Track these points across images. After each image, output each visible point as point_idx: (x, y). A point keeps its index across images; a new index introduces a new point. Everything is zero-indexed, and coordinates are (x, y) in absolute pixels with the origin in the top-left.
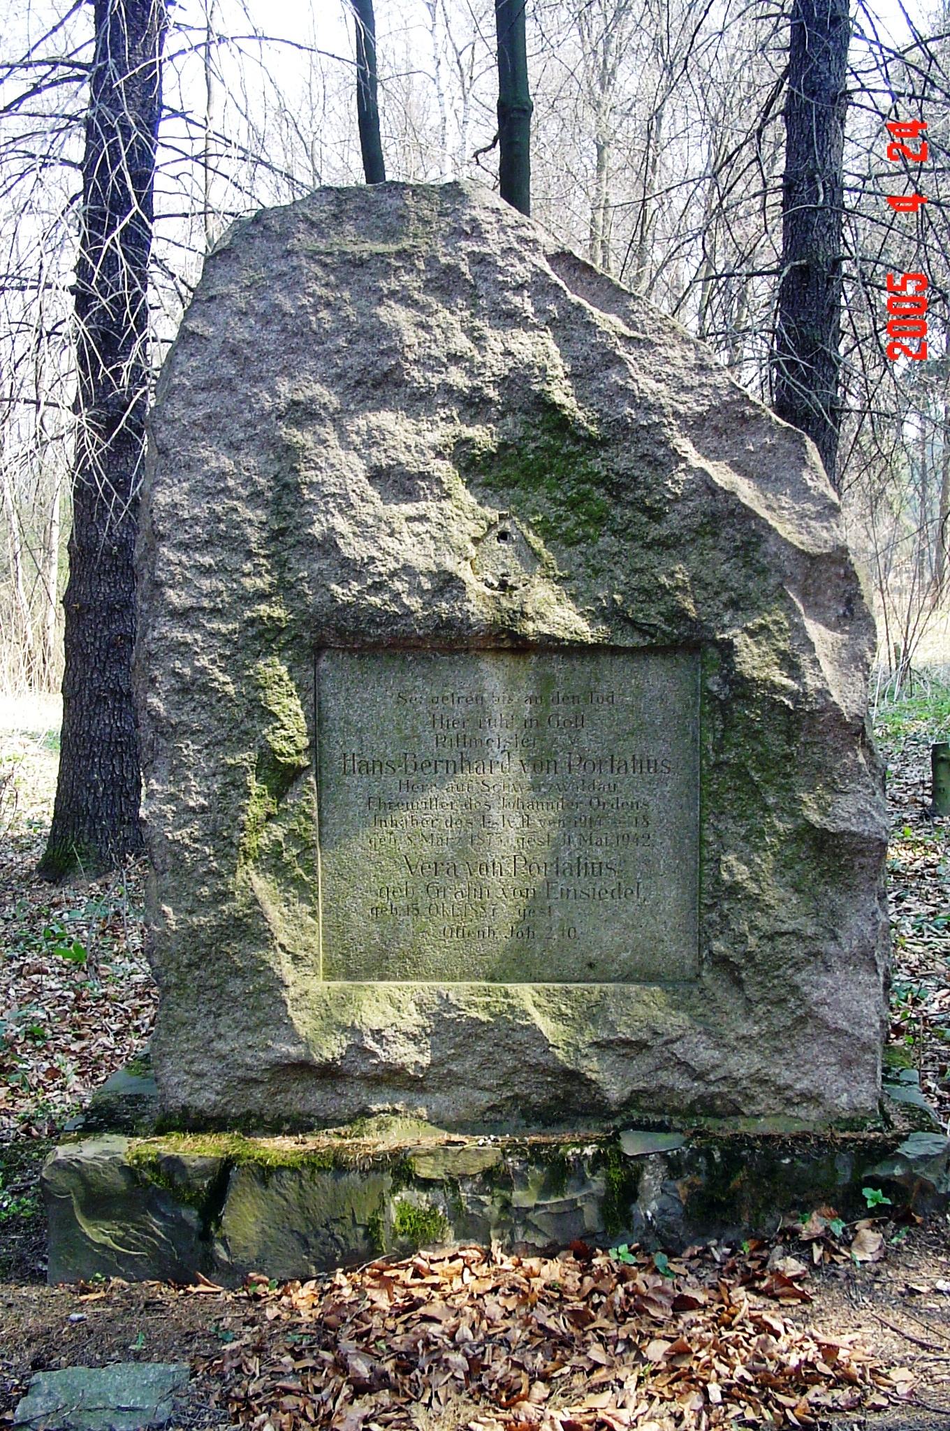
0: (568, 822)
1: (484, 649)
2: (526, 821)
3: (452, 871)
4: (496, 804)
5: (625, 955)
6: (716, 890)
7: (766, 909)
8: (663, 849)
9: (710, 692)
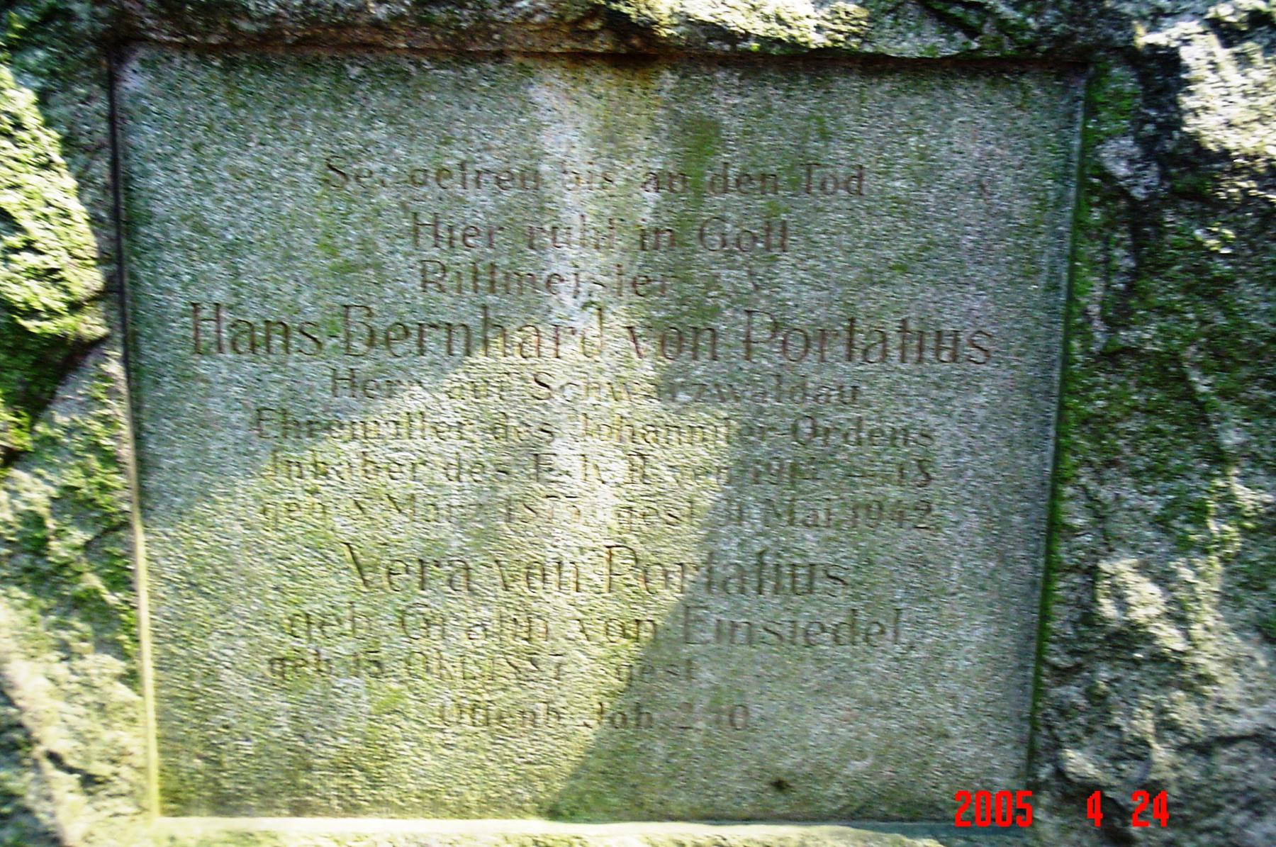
0: (744, 473)
1: (545, 56)
2: (640, 463)
3: (460, 579)
4: (566, 428)
5: (859, 765)
6: (1082, 639)
7: (1196, 685)
8: (960, 536)
9: (1108, 177)
